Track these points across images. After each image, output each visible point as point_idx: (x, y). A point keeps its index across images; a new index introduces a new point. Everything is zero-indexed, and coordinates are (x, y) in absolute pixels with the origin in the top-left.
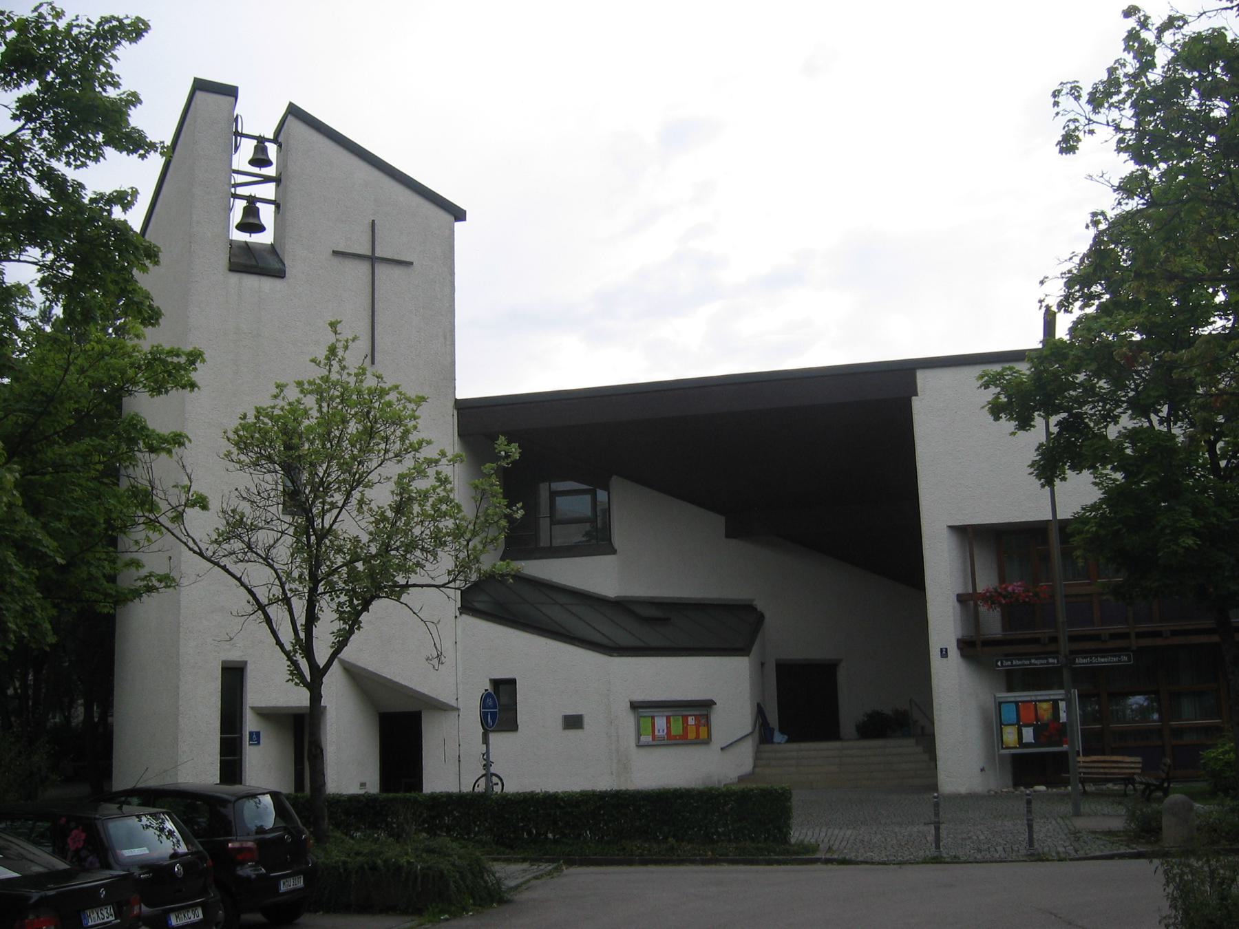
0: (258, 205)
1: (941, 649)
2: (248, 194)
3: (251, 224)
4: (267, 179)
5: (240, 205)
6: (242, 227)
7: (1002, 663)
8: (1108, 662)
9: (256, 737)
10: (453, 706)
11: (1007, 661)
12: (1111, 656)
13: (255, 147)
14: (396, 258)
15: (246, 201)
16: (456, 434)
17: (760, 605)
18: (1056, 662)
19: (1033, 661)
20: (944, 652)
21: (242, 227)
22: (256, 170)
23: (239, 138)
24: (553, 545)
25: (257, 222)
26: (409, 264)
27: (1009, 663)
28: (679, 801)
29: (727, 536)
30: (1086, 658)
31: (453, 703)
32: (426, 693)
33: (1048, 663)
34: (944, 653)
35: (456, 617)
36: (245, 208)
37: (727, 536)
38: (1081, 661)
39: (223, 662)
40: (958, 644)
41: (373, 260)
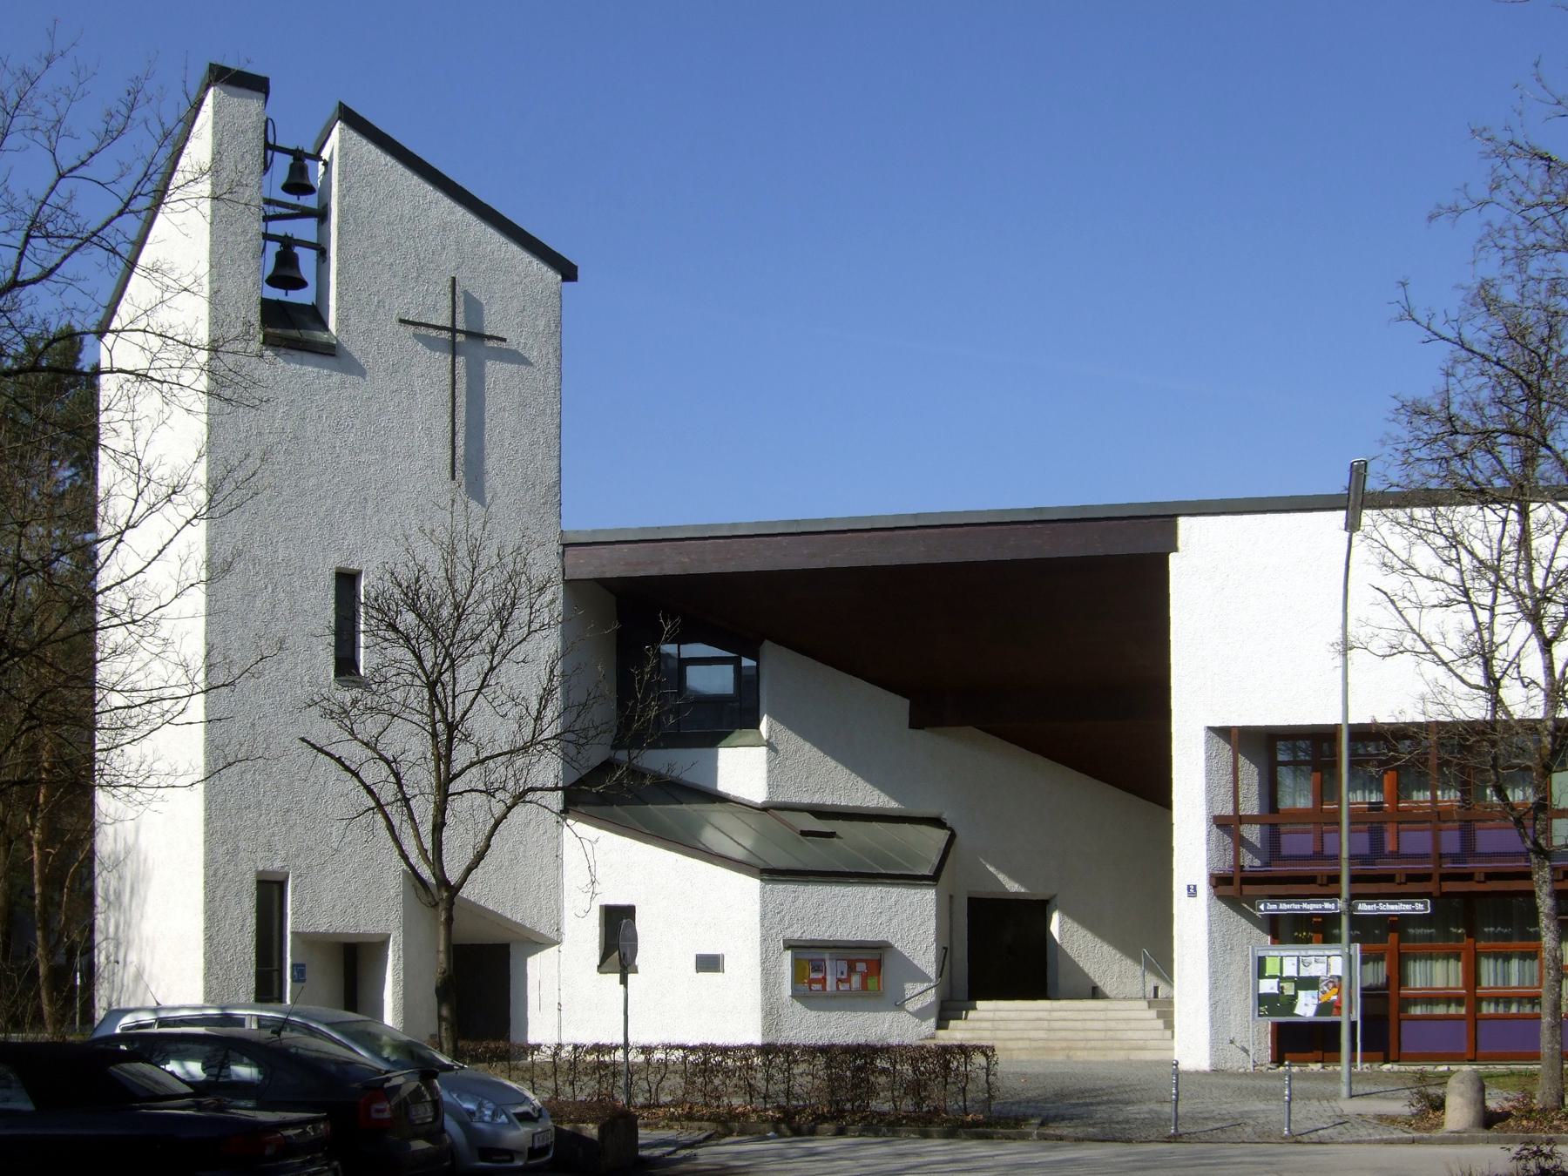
0: (297, 250)
2: (282, 234)
7: (1266, 906)
12: (1403, 903)
13: (292, 166)
15: (279, 244)
20: (1192, 891)
22: (291, 199)
23: (270, 153)
24: (1279, 768)
25: (297, 276)
30: (1371, 904)
31: (553, 936)
34: (1192, 891)
38: (1364, 908)
39: (259, 873)
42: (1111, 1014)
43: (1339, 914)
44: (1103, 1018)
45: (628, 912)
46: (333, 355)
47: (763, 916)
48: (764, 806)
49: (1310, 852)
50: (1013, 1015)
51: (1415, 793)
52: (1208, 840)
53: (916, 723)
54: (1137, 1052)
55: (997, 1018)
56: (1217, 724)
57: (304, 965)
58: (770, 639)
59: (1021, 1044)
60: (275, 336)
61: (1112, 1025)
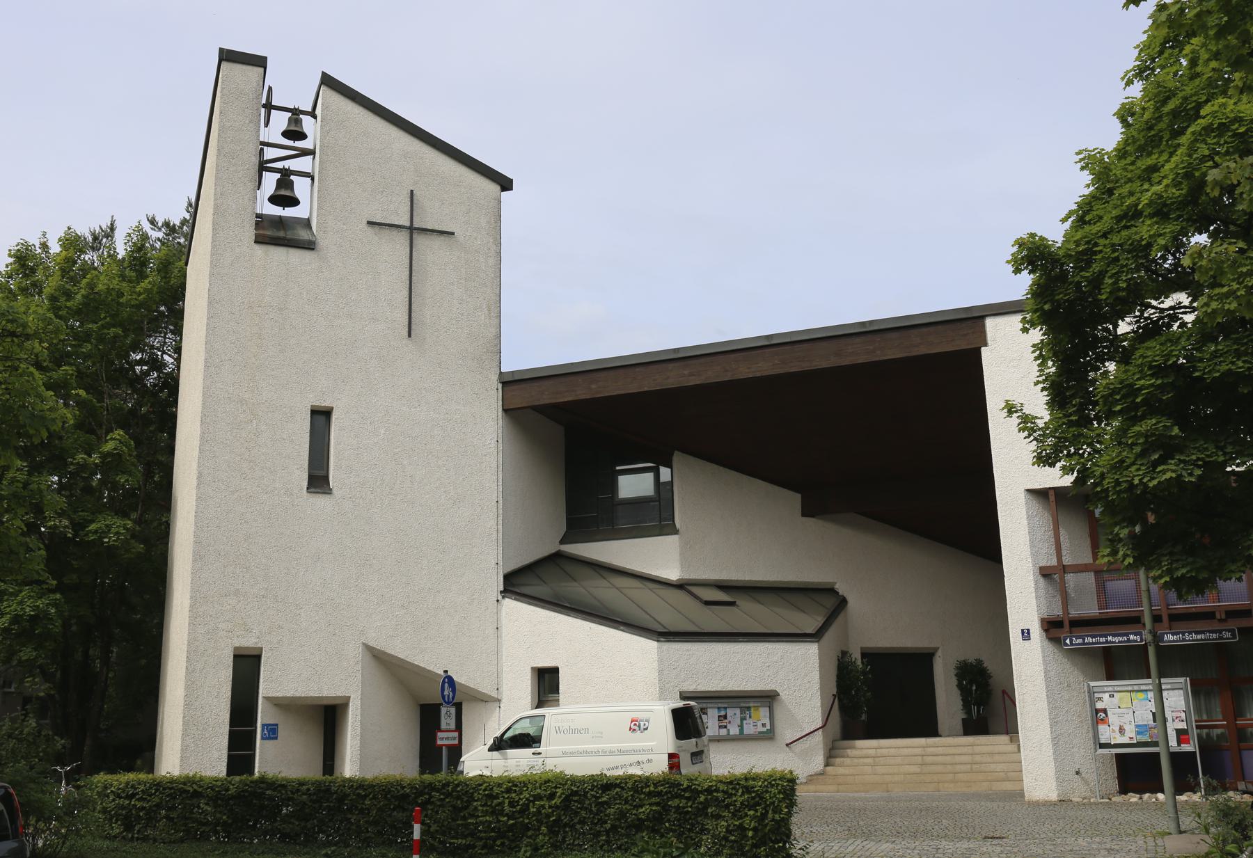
1: (1022, 630)
3: (284, 198)
4: (304, 153)
5: (270, 180)
6: (274, 200)
7: (1071, 641)
8: (1205, 640)
9: (272, 732)
10: (493, 697)
11: (1077, 638)
14: (436, 228)
16: (500, 410)
17: (841, 588)
18: (1139, 640)
19: (1110, 638)
21: (274, 200)
22: (290, 143)
26: (453, 234)
27: (1080, 641)
28: (125, 854)
29: (804, 515)
31: (494, 694)
32: (463, 683)
33: (1129, 641)
34: (1026, 635)
35: (498, 601)
36: (278, 180)
37: (804, 515)
38: (1170, 638)
39: (236, 649)
40: (1042, 624)
41: (413, 230)
42: (977, 749)
43: (1145, 646)
44: (970, 752)
45: (554, 671)
46: (313, 249)
47: (660, 673)
48: (679, 583)
49: (310, 181)
50: (893, 751)
51: (1177, 427)
52: (1036, 589)
53: (805, 513)
54: (998, 783)
55: (879, 755)
56: (1037, 486)
57: (277, 725)
58: (678, 450)
59: (896, 778)
60: (264, 236)
61: (978, 758)
